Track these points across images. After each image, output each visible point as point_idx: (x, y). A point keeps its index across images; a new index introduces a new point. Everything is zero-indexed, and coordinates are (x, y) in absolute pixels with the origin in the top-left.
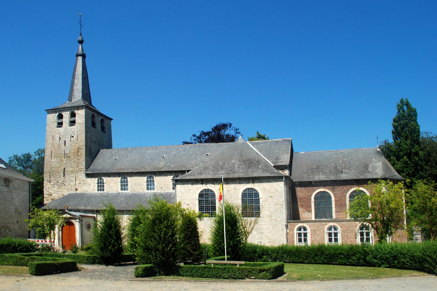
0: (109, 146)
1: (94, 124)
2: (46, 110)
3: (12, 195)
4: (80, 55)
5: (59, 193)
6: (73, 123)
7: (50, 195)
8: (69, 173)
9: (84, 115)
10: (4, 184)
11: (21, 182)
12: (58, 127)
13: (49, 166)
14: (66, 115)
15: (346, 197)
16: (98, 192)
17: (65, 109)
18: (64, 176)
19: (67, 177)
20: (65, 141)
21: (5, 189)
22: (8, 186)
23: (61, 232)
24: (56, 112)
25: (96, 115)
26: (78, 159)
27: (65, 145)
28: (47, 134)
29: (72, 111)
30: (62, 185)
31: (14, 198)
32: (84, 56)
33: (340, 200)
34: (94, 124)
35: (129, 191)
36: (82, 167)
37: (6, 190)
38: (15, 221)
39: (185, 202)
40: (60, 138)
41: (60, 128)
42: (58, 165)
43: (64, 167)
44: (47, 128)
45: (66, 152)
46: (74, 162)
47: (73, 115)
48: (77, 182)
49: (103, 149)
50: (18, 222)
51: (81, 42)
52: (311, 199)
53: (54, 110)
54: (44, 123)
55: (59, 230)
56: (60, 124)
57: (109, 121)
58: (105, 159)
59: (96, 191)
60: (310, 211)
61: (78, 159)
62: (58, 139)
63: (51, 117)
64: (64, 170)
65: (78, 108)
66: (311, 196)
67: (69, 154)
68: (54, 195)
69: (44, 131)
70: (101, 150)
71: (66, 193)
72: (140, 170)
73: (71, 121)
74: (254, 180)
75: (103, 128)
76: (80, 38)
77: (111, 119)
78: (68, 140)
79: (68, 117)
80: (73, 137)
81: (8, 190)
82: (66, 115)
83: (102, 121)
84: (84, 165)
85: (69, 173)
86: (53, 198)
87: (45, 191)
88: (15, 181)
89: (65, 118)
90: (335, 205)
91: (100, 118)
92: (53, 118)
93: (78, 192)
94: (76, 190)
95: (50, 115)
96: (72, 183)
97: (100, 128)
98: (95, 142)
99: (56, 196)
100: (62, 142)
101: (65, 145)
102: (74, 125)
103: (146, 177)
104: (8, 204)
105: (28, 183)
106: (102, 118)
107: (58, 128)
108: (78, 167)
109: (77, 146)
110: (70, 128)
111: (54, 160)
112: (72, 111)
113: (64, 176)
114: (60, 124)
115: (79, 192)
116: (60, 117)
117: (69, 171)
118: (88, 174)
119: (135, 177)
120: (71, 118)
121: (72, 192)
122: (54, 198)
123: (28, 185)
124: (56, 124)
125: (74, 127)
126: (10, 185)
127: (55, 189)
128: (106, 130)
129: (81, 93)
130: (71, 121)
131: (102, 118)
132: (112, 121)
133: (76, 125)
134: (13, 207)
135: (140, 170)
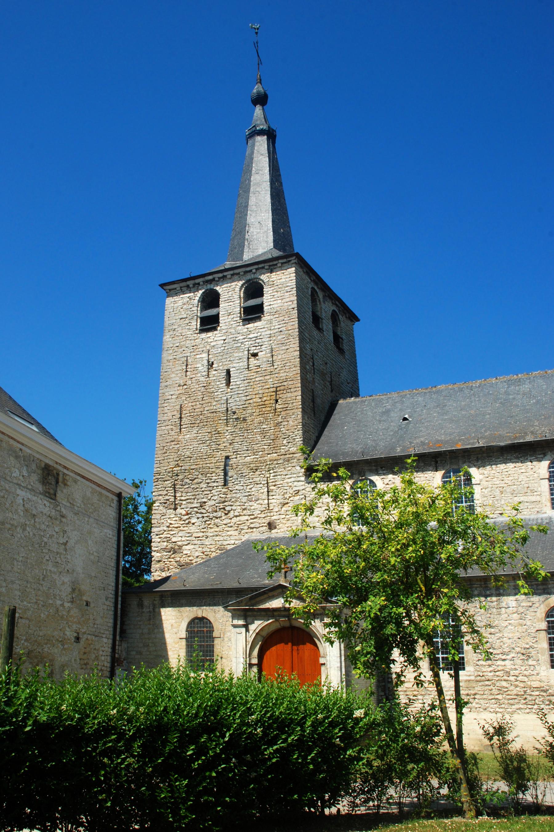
0: (355, 393)
1: (316, 320)
2: (162, 286)
3: (65, 532)
4: (261, 133)
5: (207, 542)
6: (252, 313)
7: (175, 550)
8: (246, 471)
9: (293, 284)
10: (40, 487)
11: (93, 492)
12: (202, 331)
13: (174, 456)
14: (231, 295)
17: (225, 275)
18: (225, 484)
19: (236, 485)
20: (228, 372)
21: (43, 505)
22: (52, 496)
24: (196, 287)
25: (321, 295)
26: (278, 424)
27: (228, 383)
28: (166, 356)
29: (249, 276)
30: (219, 514)
31: (71, 543)
32: (271, 135)
34: (316, 320)
36: (293, 449)
37: (46, 510)
38: (70, 634)
40: (211, 365)
41: (210, 334)
42: (204, 449)
43: (225, 454)
44: (167, 338)
45: (233, 406)
46: (263, 433)
47: (254, 290)
48: (275, 501)
49: (345, 398)
50: (78, 639)
51: (261, 100)
53: (190, 283)
54: (153, 329)
55: (251, 665)
56: (209, 323)
58: (361, 424)
61: (278, 424)
62: (202, 367)
63: (180, 303)
64: (226, 465)
65: (270, 264)
67: (244, 409)
68: (186, 550)
69: (157, 347)
70: (341, 402)
71: (232, 539)
72: (520, 438)
73: (245, 308)
76: (257, 89)
78: (237, 367)
79: (236, 296)
80: (255, 355)
81: (53, 513)
82: (231, 295)
84: (299, 440)
85: (246, 471)
86: (184, 560)
87: (155, 539)
88: (76, 481)
89: (229, 300)
92: (183, 307)
94: (271, 526)
95: (176, 298)
96: (255, 505)
97: (331, 338)
98: (323, 374)
99: (193, 552)
100: (218, 375)
101: (228, 383)
102: (259, 318)
103: (545, 464)
104: (50, 567)
105: (115, 498)
107: (204, 335)
108: (275, 448)
109: (271, 381)
110: (243, 329)
111: (188, 435)
112: (249, 276)
113: (225, 484)
114: (209, 323)
115: (281, 535)
116: (211, 300)
117: (244, 464)
119: (502, 466)
120: (245, 301)
121: (255, 535)
122: (187, 560)
123: (115, 504)
124: (196, 324)
125: (258, 324)
126: (59, 495)
127: (193, 529)
129: (271, 233)
130: (245, 308)
133: (266, 318)
134: (67, 579)
135: (520, 438)
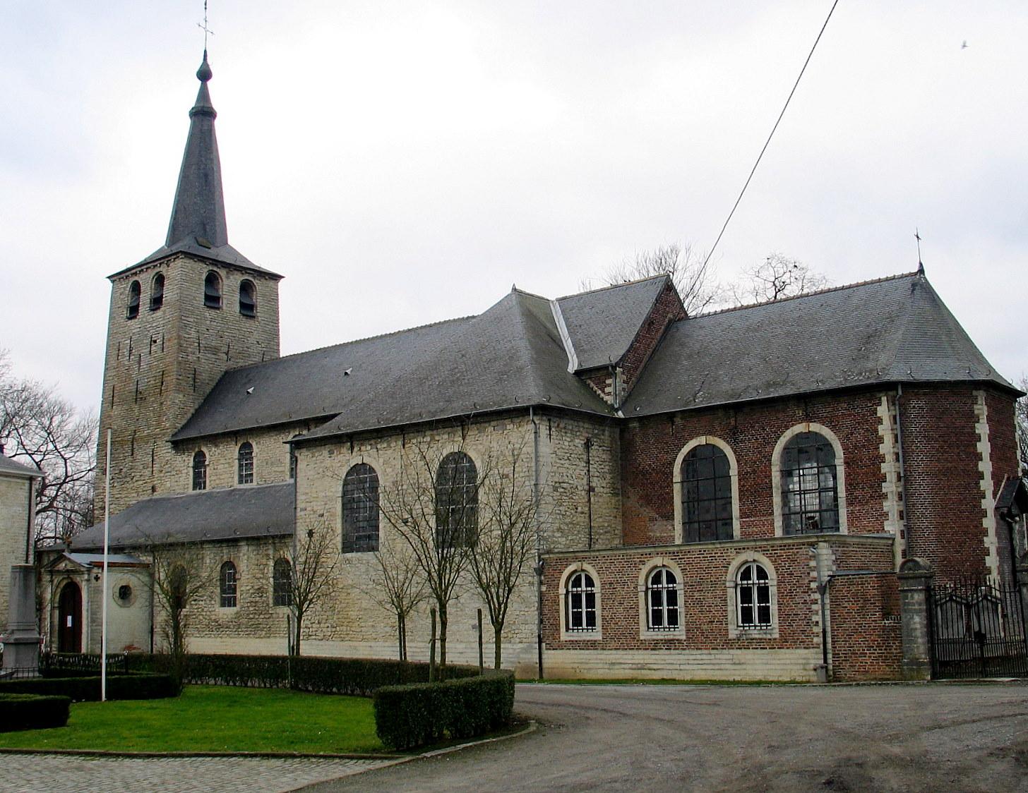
15: (770, 460)
16: (195, 491)
23: (57, 612)
30: (128, 479)
33: (754, 472)
35: (254, 485)
39: (315, 508)
52: (672, 473)
53: (123, 275)
57: (271, 283)
59: (191, 491)
60: (669, 517)
66: (671, 464)
74: (461, 423)
75: (247, 309)
77: (276, 278)
83: (246, 288)
90: (740, 491)
91: (236, 280)
93: (157, 495)
94: (154, 489)
105: (27, 482)
106: (246, 277)
108: (159, 424)
115: (158, 497)
118: (177, 441)
128: (260, 311)
131: (246, 277)
132: (281, 283)
